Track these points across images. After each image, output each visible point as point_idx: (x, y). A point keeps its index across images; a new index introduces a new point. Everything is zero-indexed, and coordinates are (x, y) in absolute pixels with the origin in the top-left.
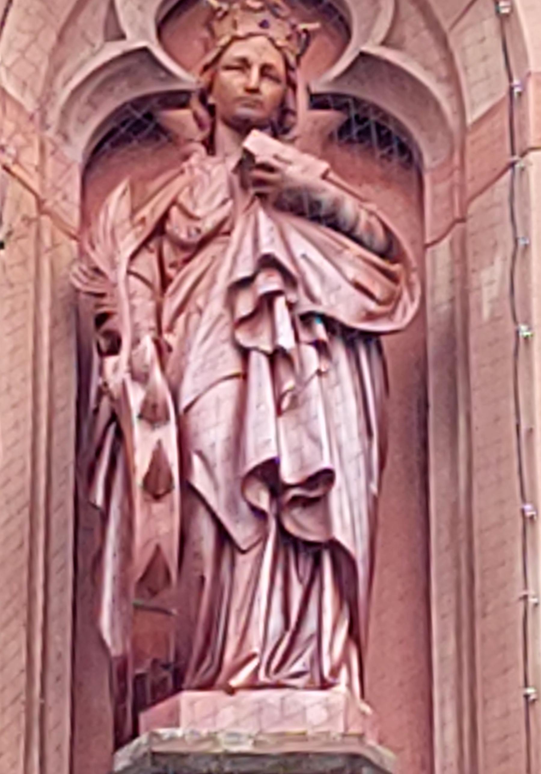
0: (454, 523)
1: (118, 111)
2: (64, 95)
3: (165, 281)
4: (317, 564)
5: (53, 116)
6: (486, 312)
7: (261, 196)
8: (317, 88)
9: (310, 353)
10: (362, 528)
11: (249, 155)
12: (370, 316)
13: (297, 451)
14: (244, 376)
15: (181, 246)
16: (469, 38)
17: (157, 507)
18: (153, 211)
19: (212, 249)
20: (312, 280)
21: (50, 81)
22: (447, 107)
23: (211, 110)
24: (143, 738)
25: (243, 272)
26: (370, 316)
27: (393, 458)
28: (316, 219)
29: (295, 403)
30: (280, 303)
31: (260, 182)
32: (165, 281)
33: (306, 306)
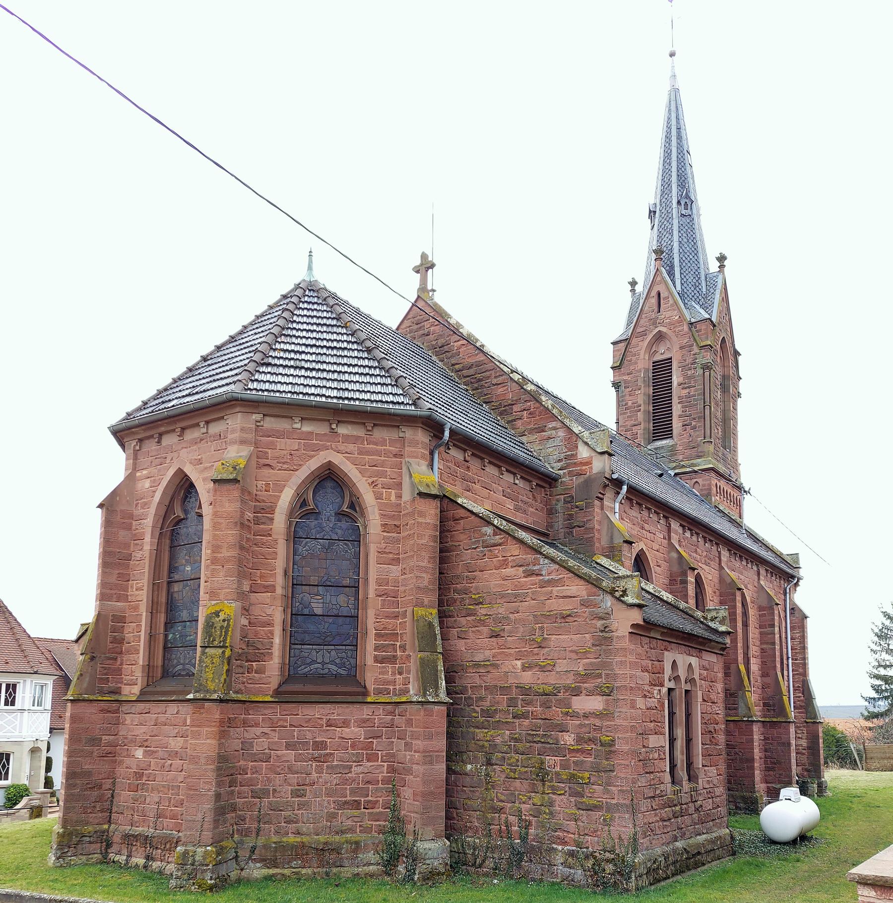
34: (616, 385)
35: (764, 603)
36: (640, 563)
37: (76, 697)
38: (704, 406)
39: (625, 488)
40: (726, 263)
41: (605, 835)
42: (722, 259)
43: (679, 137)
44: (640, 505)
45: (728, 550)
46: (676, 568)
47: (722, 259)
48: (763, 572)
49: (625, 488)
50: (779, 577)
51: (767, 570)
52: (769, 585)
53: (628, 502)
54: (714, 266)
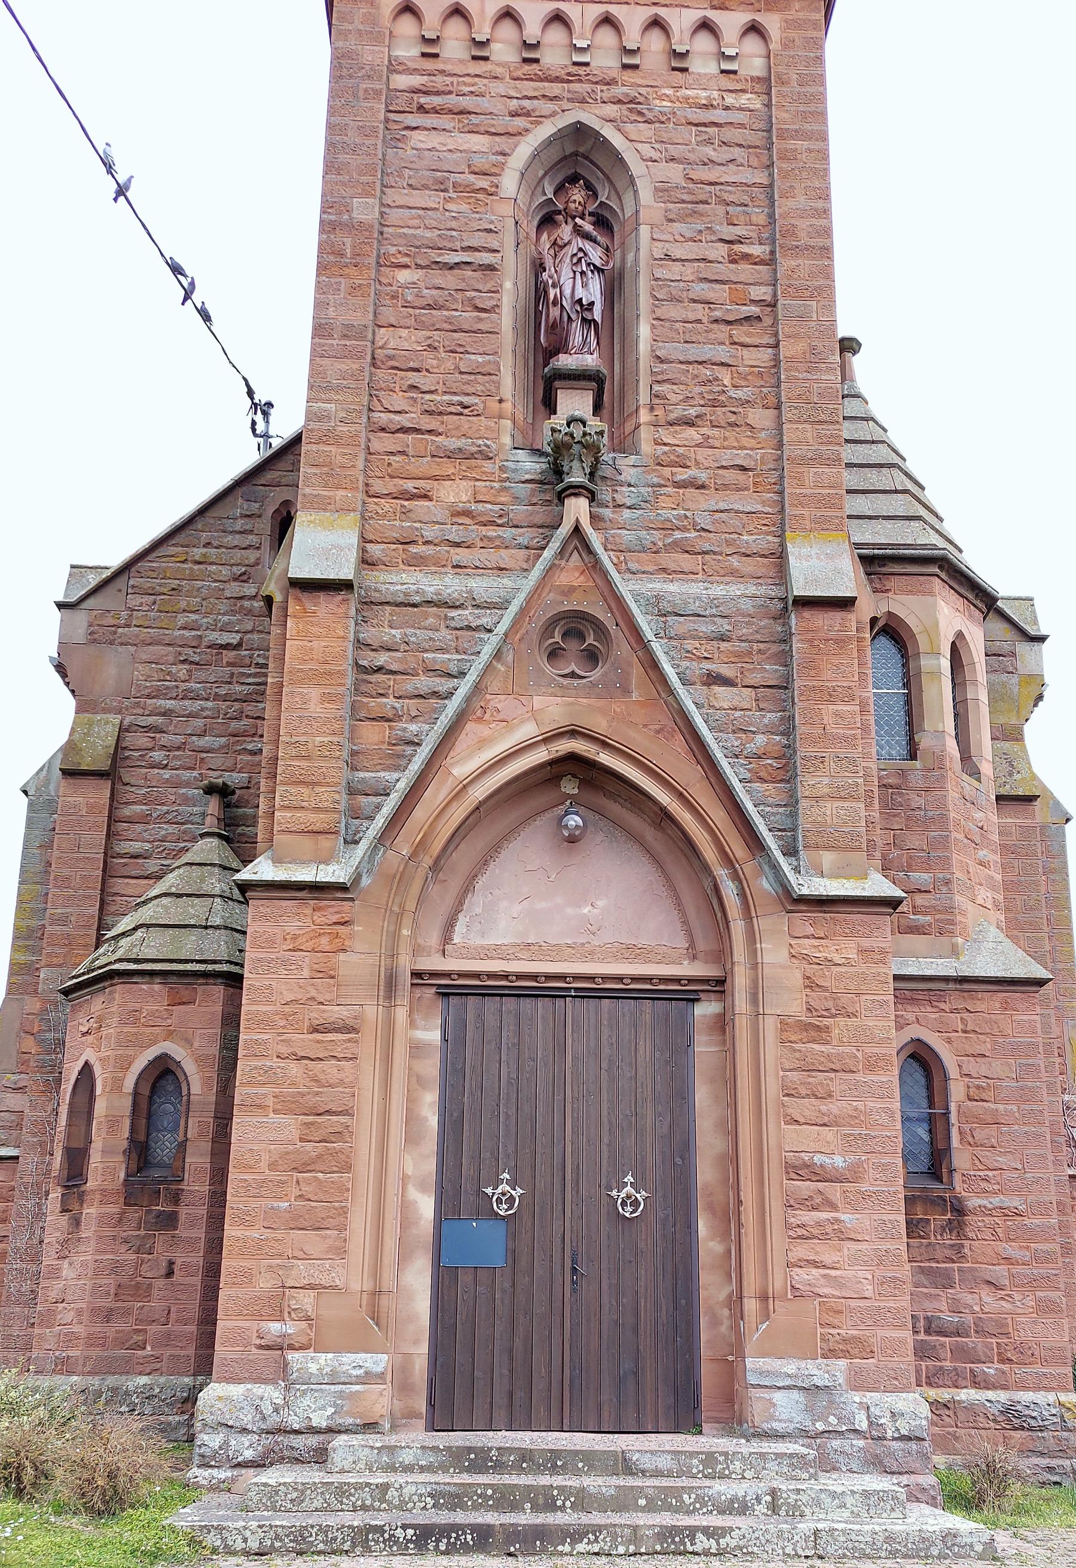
0: (620, 323)
1: (544, 216)
2: (531, 211)
3: (556, 255)
4: (590, 326)
5: (530, 214)
6: (629, 265)
7: (578, 234)
8: (590, 210)
9: (590, 273)
10: (600, 316)
11: (576, 223)
12: (603, 265)
13: (586, 296)
14: (574, 278)
15: (560, 247)
16: (627, 196)
17: (555, 308)
18: (446, 716)
19: (568, 247)
20: (590, 255)
21: (530, 203)
22: (620, 214)
23: (566, 213)
24: (551, 365)
25: (575, 252)
26: (603, 265)
27: (602, 342)
28: (591, 240)
29: (586, 285)
30: (583, 260)
31: (579, 230)
32: (556, 255)
33: (589, 261)
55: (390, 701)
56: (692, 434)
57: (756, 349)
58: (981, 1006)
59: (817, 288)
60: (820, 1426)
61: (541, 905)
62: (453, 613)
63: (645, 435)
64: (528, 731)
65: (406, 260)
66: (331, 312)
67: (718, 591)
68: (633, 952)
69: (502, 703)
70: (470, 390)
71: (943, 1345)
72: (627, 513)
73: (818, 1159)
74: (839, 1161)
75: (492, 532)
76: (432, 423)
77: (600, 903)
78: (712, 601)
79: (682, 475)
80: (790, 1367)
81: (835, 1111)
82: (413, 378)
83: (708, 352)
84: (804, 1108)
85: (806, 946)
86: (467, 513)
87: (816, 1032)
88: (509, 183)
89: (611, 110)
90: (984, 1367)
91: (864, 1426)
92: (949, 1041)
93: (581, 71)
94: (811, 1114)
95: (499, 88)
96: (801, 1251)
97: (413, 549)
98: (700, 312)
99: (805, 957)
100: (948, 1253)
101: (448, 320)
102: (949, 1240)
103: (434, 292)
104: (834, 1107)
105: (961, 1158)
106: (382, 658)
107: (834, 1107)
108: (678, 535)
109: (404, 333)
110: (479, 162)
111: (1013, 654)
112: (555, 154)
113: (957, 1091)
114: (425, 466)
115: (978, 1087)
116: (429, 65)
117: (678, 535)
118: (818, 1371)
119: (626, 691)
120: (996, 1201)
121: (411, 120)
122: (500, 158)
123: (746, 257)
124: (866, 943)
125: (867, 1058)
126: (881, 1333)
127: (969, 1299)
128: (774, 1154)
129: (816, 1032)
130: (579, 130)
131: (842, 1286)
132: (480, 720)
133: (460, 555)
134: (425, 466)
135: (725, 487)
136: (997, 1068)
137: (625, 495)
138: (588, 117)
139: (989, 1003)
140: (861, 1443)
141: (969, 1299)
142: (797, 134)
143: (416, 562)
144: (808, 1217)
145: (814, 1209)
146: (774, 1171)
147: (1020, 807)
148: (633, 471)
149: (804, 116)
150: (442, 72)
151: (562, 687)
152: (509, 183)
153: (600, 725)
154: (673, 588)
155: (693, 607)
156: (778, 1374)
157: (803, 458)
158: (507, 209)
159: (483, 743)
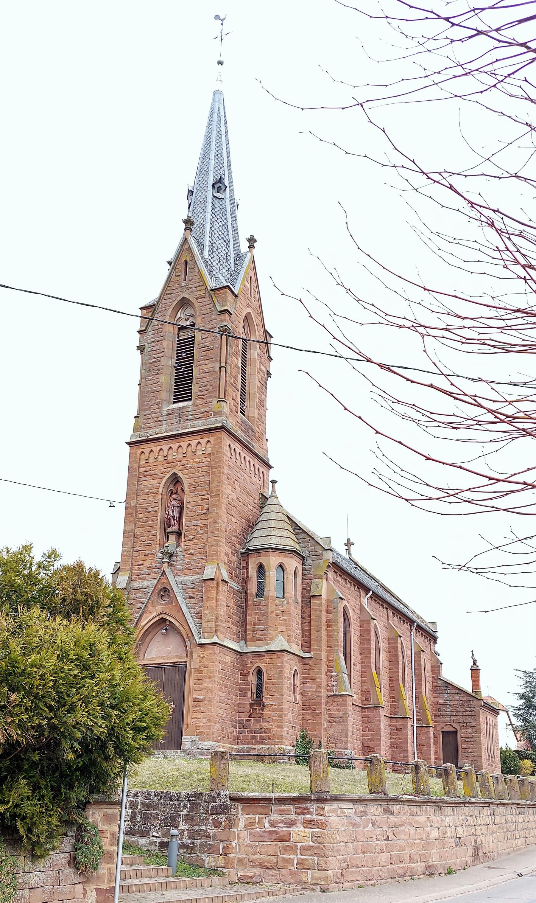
34: (141, 349)
35: (435, 664)
36: (346, 617)
37: (376, 711)
38: (220, 368)
39: (371, 592)
40: (255, 245)
41: (300, 778)
42: (252, 241)
43: (219, 144)
44: (375, 600)
45: (335, 571)
46: (435, 664)
47: (252, 241)
48: (390, 614)
49: (371, 592)
50: (374, 599)
51: (393, 613)
52: (418, 639)
53: (370, 598)
54: (244, 246)
55: (134, 610)
56: (192, 542)
57: (495, 309)
58: (272, 657)
59: (216, 505)
60: (193, 748)
61: (160, 648)
62: (145, 590)
63: (183, 544)
64: (155, 614)
65: (141, 512)
66: (127, 528)
67: (193, 578)
68: (169, 658)
69: (150, 609)
70: (151, 539)
71: (258, 736)
72: (178, 563)
73: (198, 697)
74: (202, 697)
75: (153, 571)
76: (144, 548)
77: (171, 647)
78: (192, 580)
79: (189, 552)
80: (189, 737)
81: (202, 687)
82: (141, 539)
83: (196, 523)
84: (197, 687)
85: (200, 654)
86: (150, 567)
87: (200, 671)
88: (160, 490)
89: (180, 468)
90: (265, 740)
91: (200, 747)
92: (265, 666)
93: (175, 460)
94: (198, 688)
95: (160, 467)
96: (194, 715)
97: (140, 577)
98: (194, 513)
99: (200, 656)
100: (260, 715)
101: (148, 525)
102: (261, 712)
103: (146, 519)
104: (202, 687)
105: (265, 694)
106: (132, 602)
107: (202, 687)
108: (187, 566)
109: (140, 529)
110: (155, 486)
111: (322, 554)
112: (171, 479)
113: (265, 677)
114: (142, 558)
115: (270, 676)
116: (147, 465)
117: (187, 566)
118: (193, 738)
119: (172, 603)
120: (271, 703)
121: (143, 479)
122: (159, 484)
123: (204, 499)
124: (211, 652)
125: (209, 676)
126: (206, 730)
127: (264, 725)
128: (191, 697)
129: (200, 671)
130: (175, 474)
131: (200, 722)
132: (146, 613)
133: (148, 577)
134: (142, 558)
135: (197, 553)
136: (273, 671)
137: (179, 558)
138: (176, 471)
139: (274, 656)
140: (199, 751)
141: (264, 725)
142: (215, 467)
143: (140, 579)
144: (196, 709)
145: (197, 707)
146: (191, 700)
147: (318, 598)
148: (180, 553)
149: (216, 462)
150: (149, 466)
151: (161, 604)
152: (160, 490)
153: (167, 611)
154: (185, 578)
155: (188, 582)
156: (187, 739)
157: (211, 545)
158: (160, 496)
159: (147, 618)
